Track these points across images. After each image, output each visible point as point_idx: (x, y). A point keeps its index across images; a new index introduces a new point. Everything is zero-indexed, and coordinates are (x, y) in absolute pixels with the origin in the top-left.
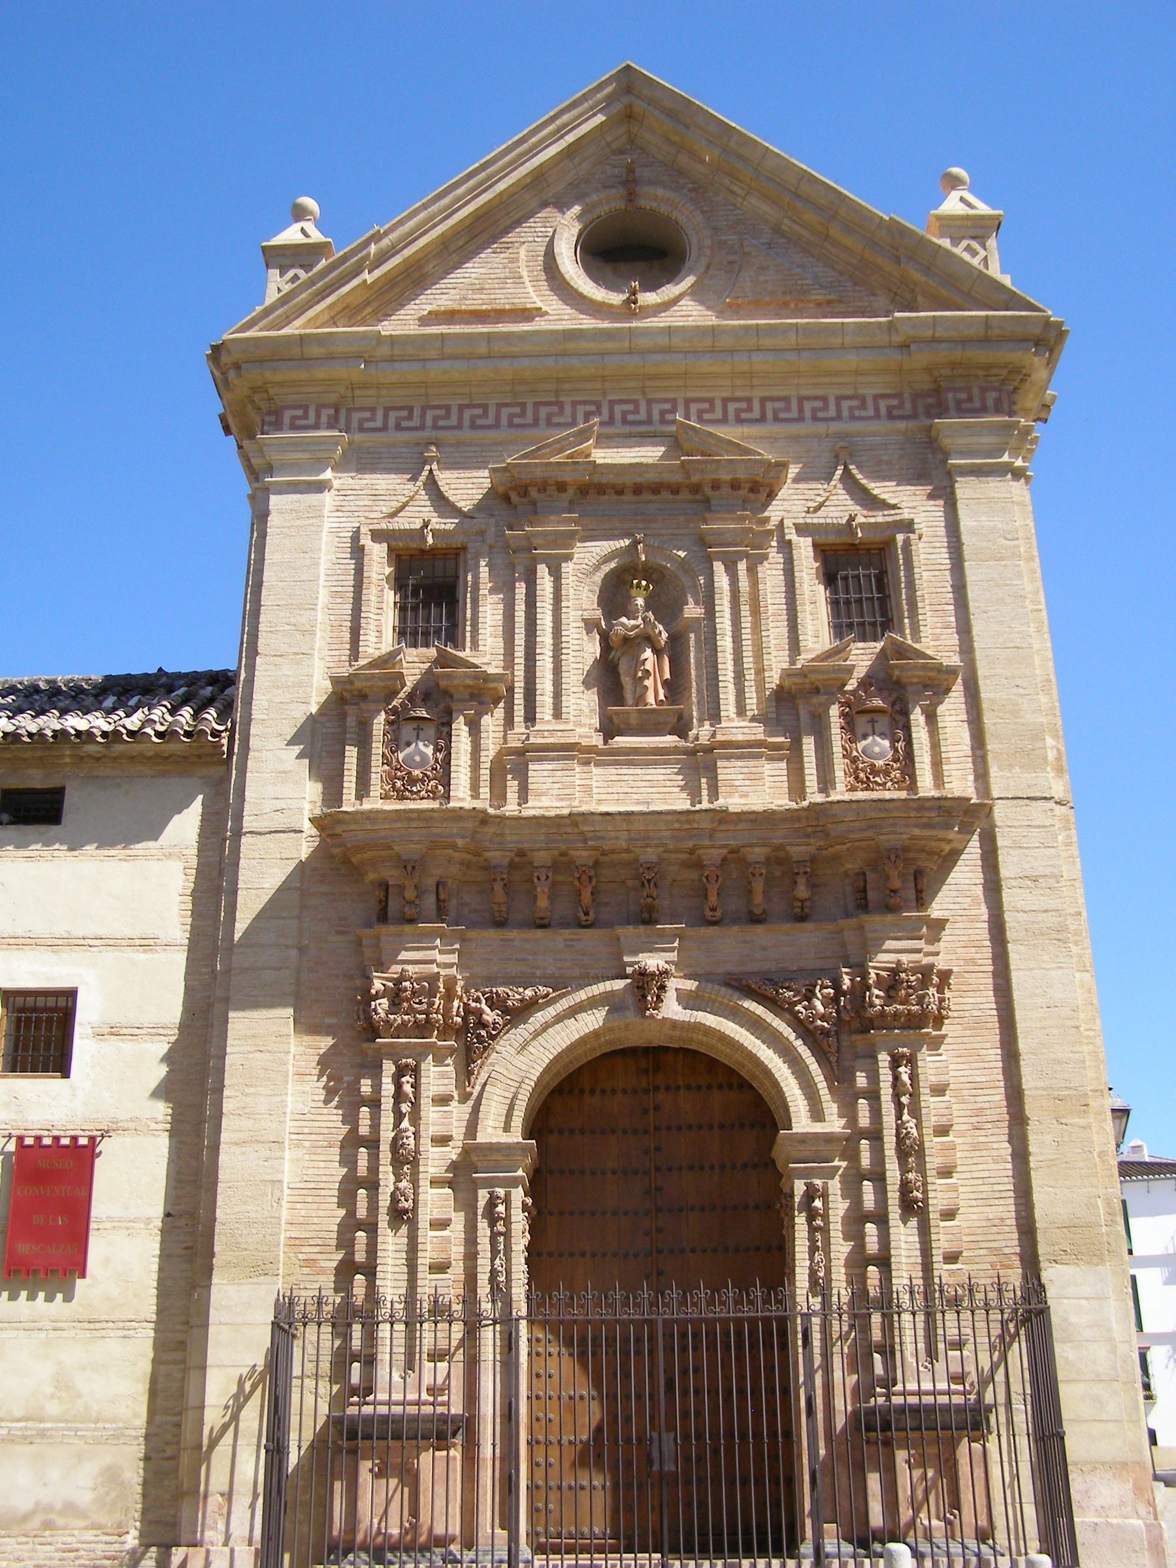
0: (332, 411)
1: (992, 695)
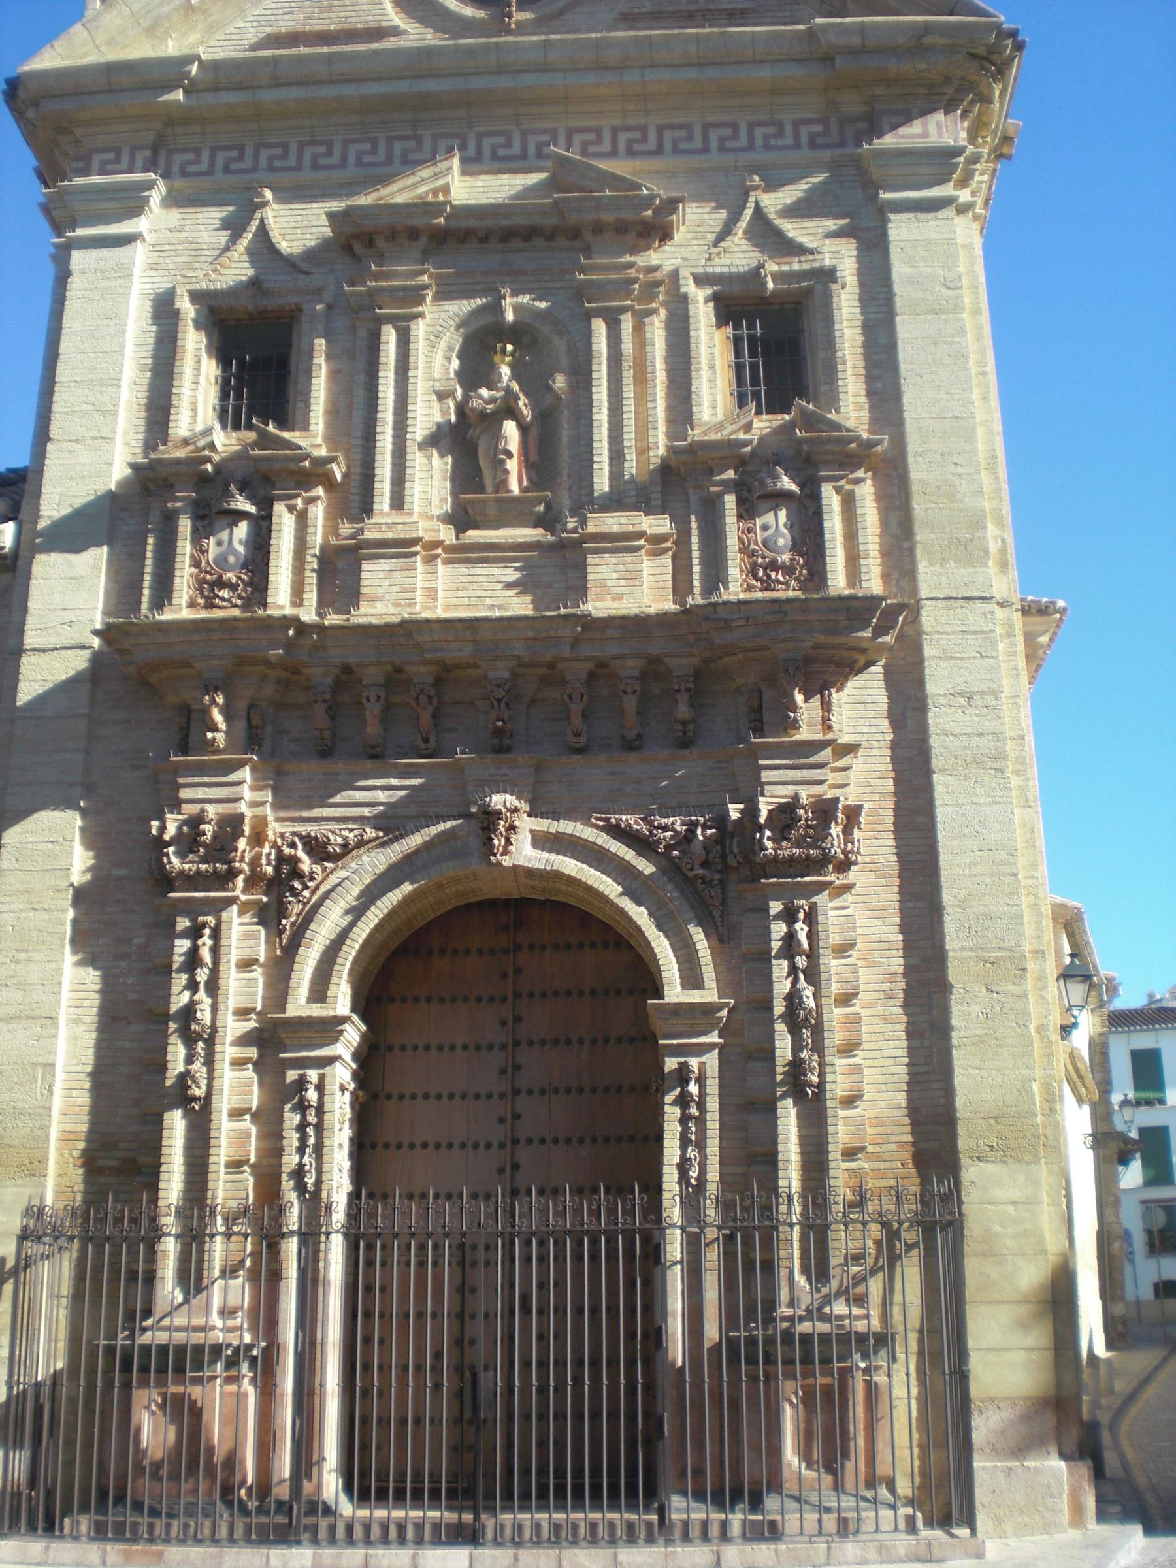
0: (148, 153)
1: (924, 475)
